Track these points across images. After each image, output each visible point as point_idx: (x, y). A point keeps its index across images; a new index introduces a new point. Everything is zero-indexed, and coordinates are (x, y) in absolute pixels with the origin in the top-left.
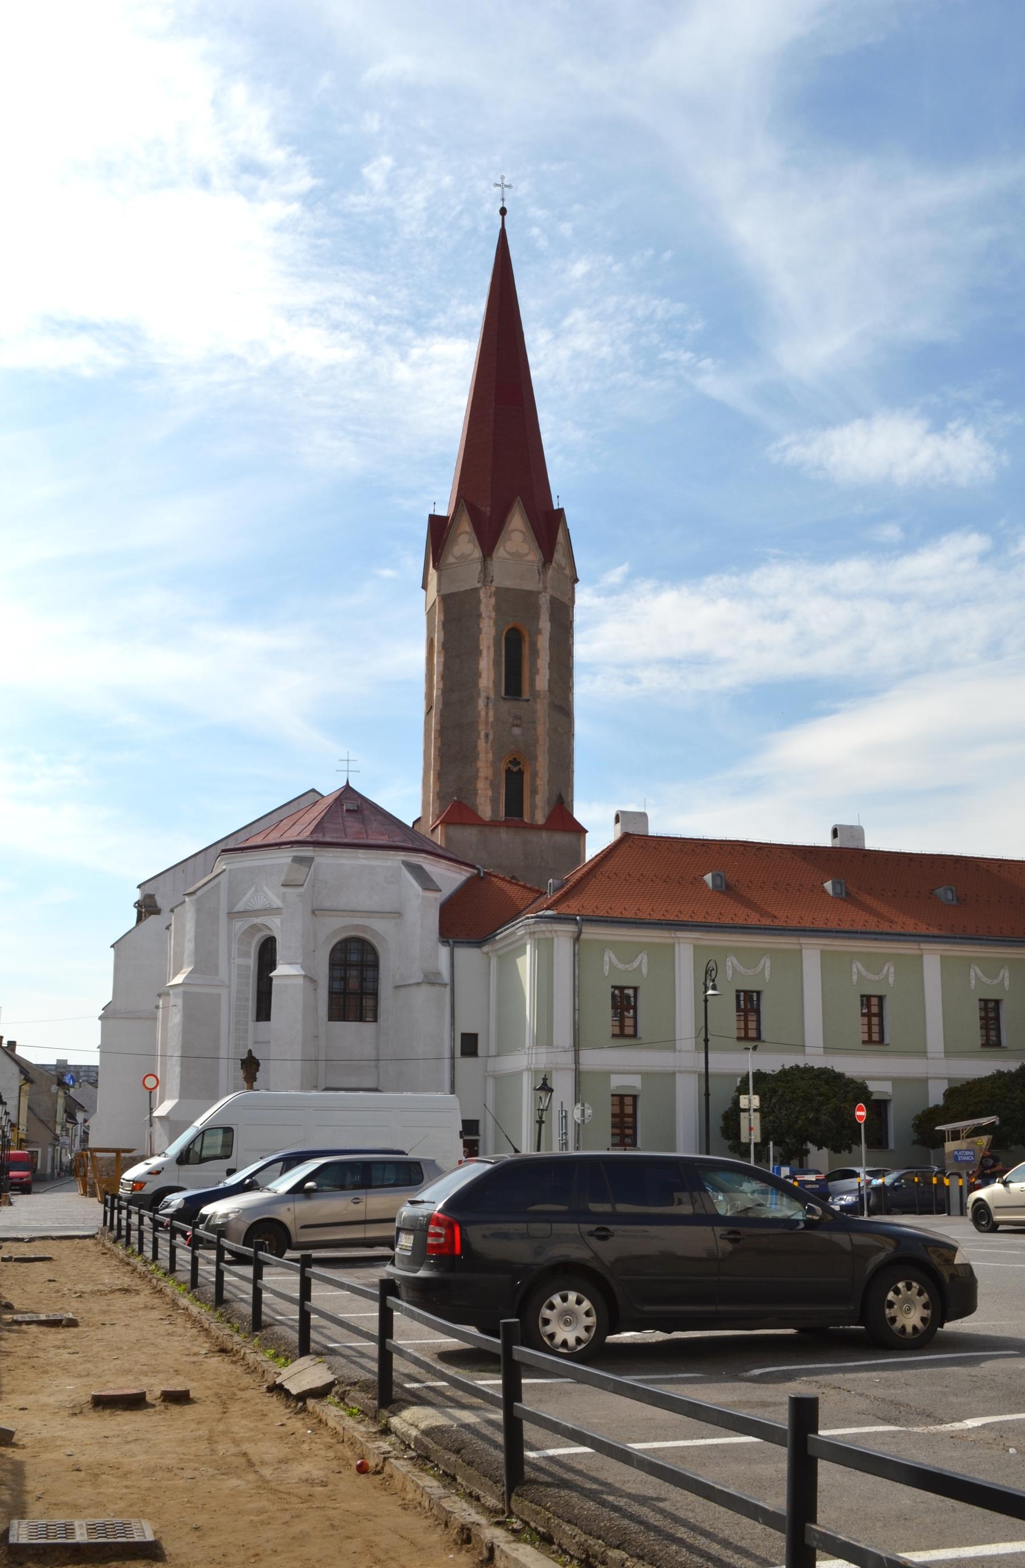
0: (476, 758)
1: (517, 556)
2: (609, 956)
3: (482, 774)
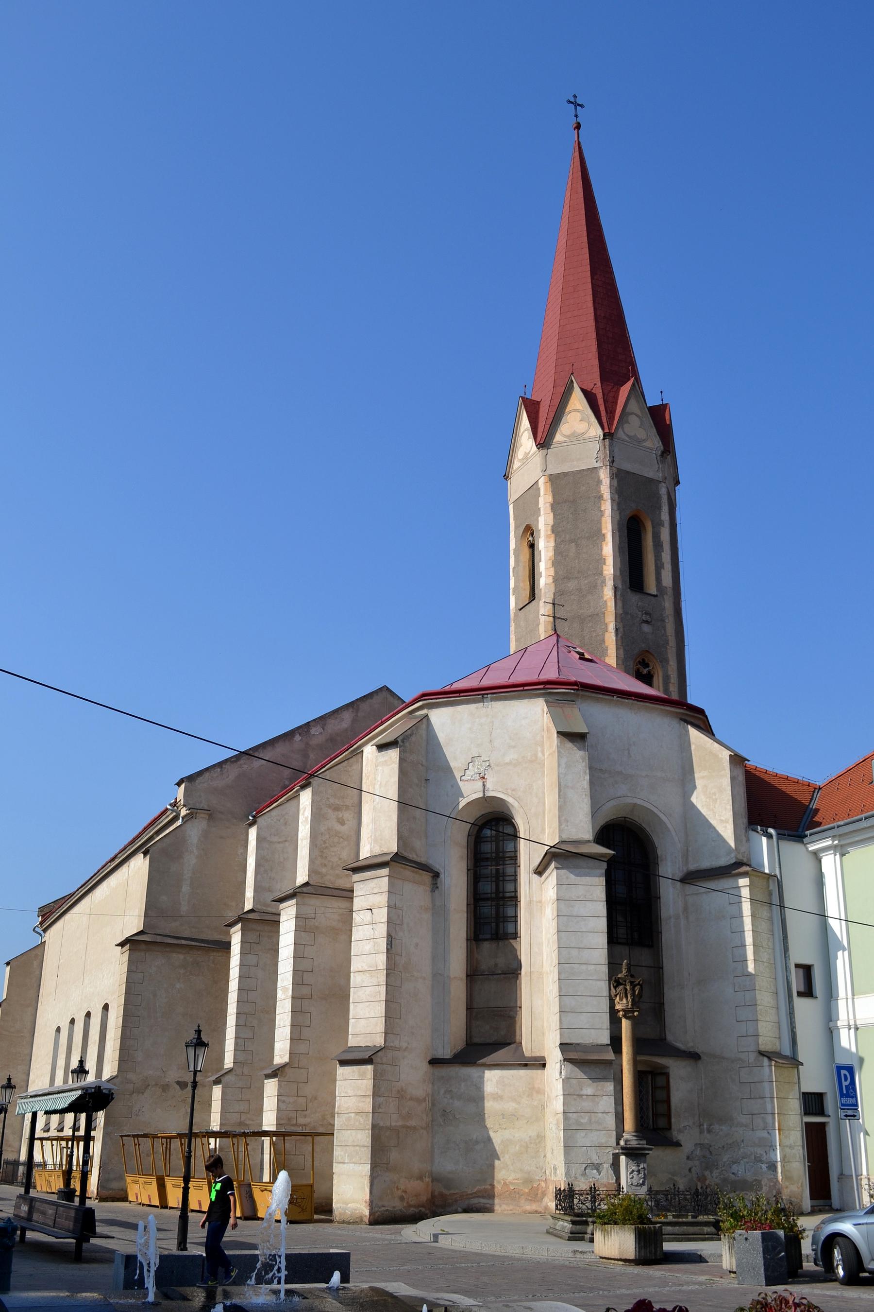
1: (575, 437)
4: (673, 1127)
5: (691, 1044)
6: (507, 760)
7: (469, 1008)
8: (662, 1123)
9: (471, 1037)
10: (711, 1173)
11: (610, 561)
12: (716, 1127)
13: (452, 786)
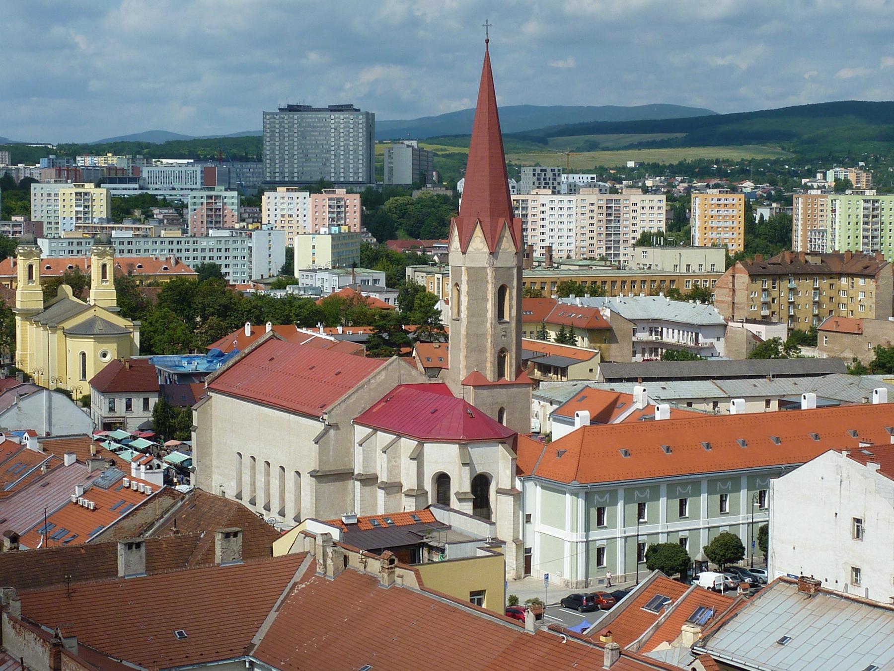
0: (486, 352)
2: (597, 497)
3: (489, 359)
11: (490, 311)
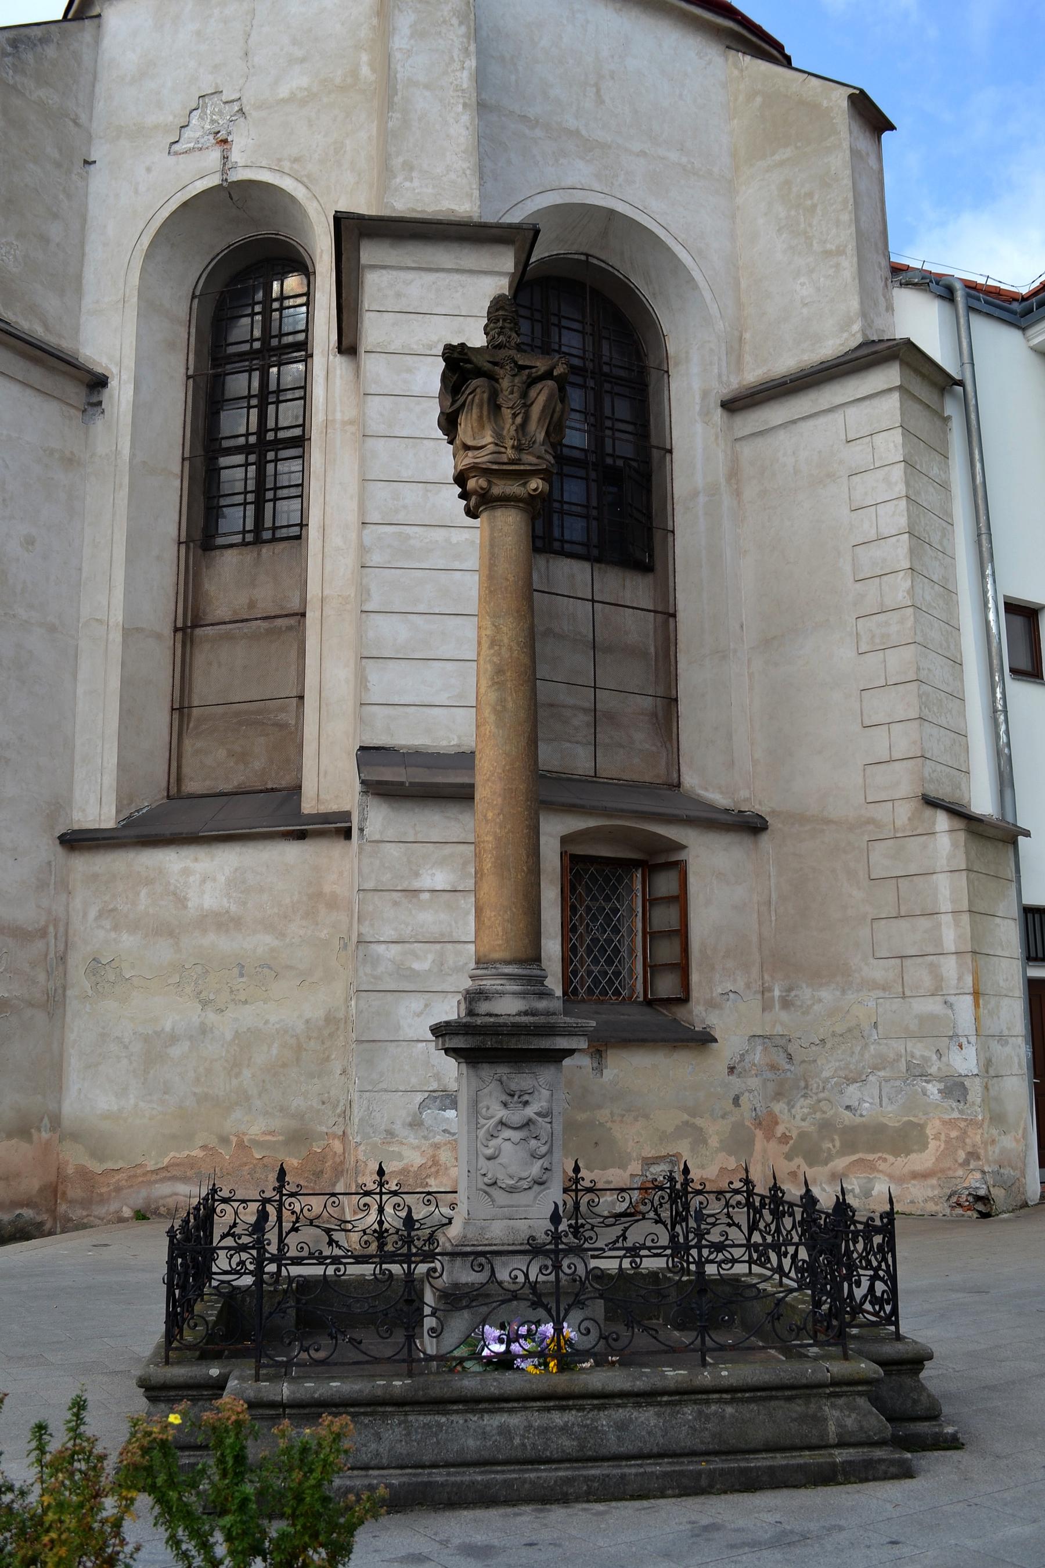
4: (695, 993)
5: (744, 794)
6: (283, 92)
7: (181, 709)
8: (666, 986)
9: (179, 780)
10: (791, 1105)
12: (805, 993)
13: (149, 170)
